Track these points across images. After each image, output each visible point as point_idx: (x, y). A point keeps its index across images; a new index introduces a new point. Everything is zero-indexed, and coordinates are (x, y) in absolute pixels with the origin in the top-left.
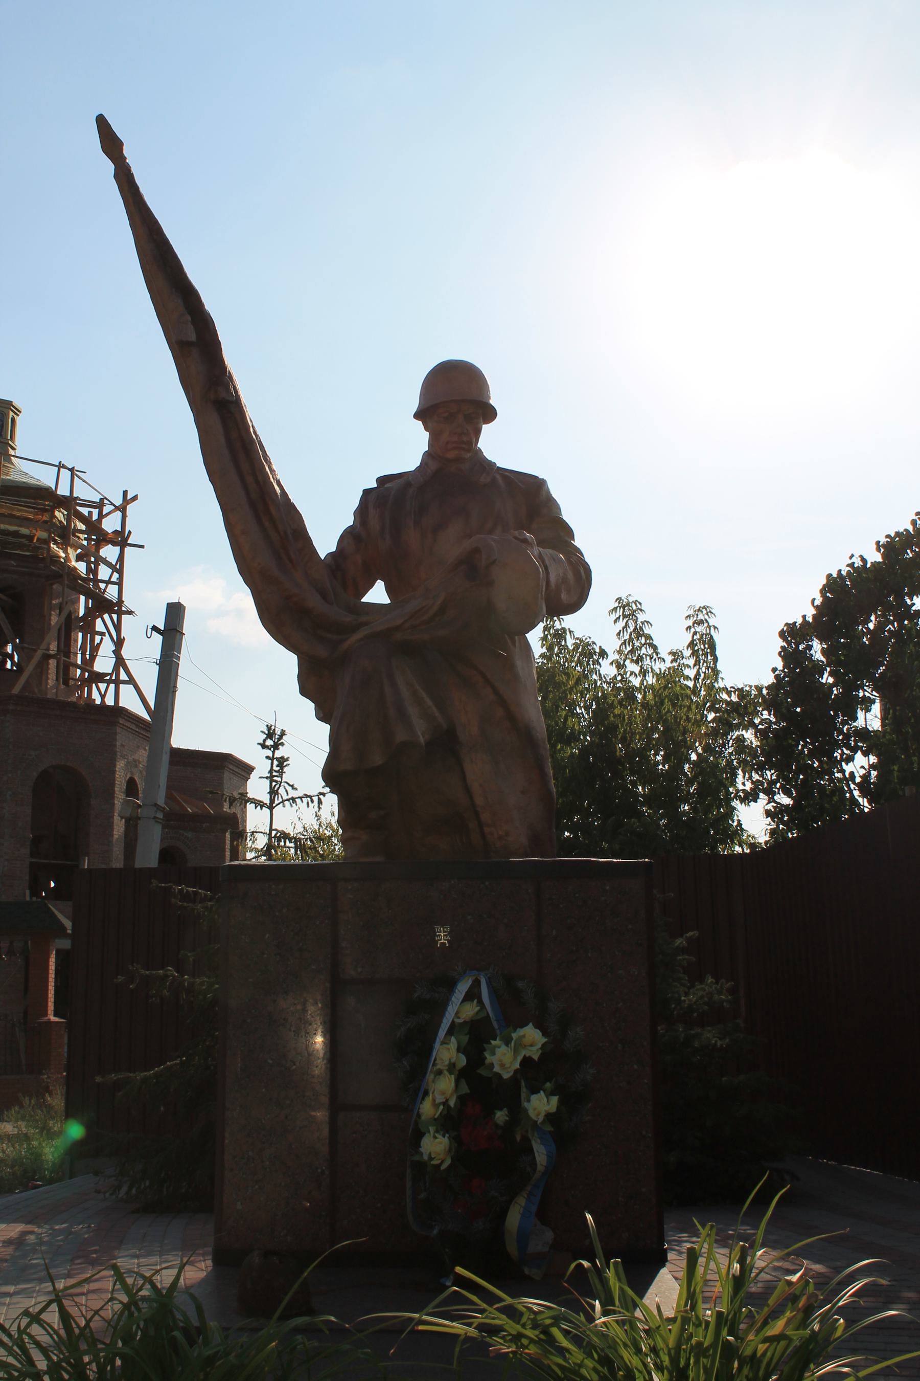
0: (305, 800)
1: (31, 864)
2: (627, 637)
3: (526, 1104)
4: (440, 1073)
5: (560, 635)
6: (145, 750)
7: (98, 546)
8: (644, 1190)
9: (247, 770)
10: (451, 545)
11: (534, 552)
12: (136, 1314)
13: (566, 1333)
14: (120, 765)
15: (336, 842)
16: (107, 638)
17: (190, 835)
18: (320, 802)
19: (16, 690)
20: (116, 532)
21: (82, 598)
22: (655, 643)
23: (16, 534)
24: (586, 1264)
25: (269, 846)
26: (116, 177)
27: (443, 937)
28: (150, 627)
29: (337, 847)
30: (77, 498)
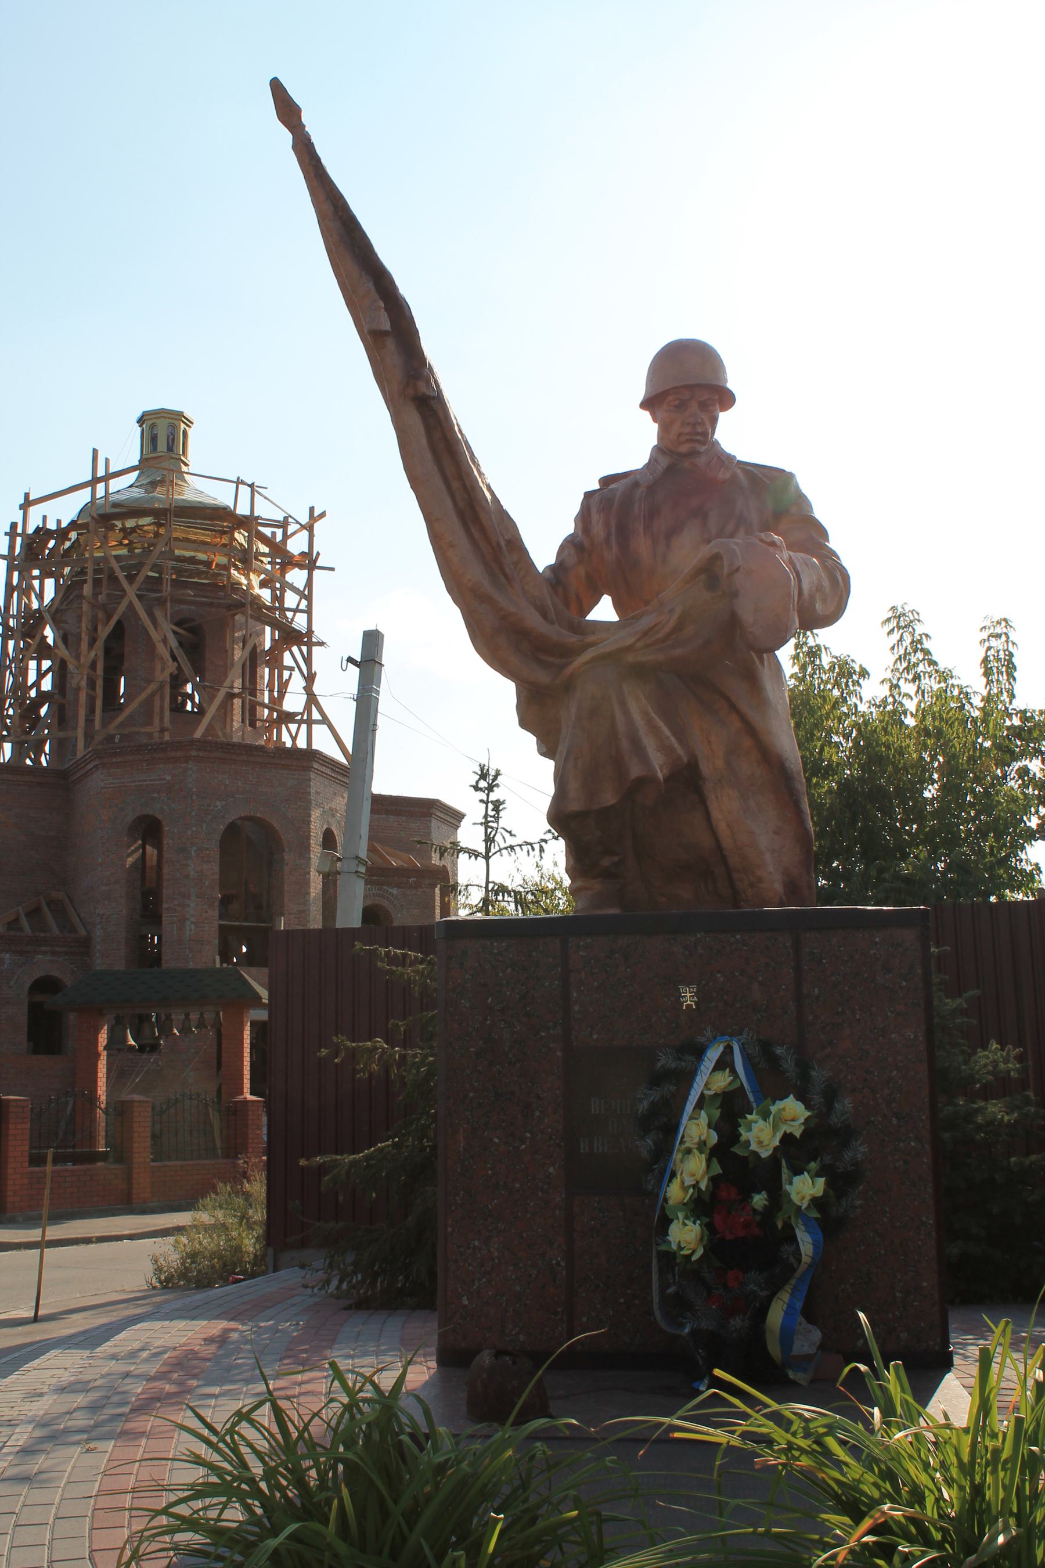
0: (525, 848)
1: (221, 926)
2: (902, 652)
3: (788, 1187)
4: (689, 1151)
5: (814, 653)
6: (343, 797)
7: (283, 571)
8: (925, 1284)
9: (455, 817)
10: (687, 552)
11: (784, 556)
12: (358, 1416)
13: (843, 1443)
14: (315, 814)
15: (560, 895)
16: (296, 673)
17: (395, 891)
18: (542, 850)
19: (198, 734)
20: (303, 554)
21: (268, 629)
22: (934, 658)
23: (192, 560)
24: (863, 1368)
25: (486, 901)
26: (294, 148)
27: (688, 998)
28: (345, 658)
29: (561, 902)
30: (258, 517)
